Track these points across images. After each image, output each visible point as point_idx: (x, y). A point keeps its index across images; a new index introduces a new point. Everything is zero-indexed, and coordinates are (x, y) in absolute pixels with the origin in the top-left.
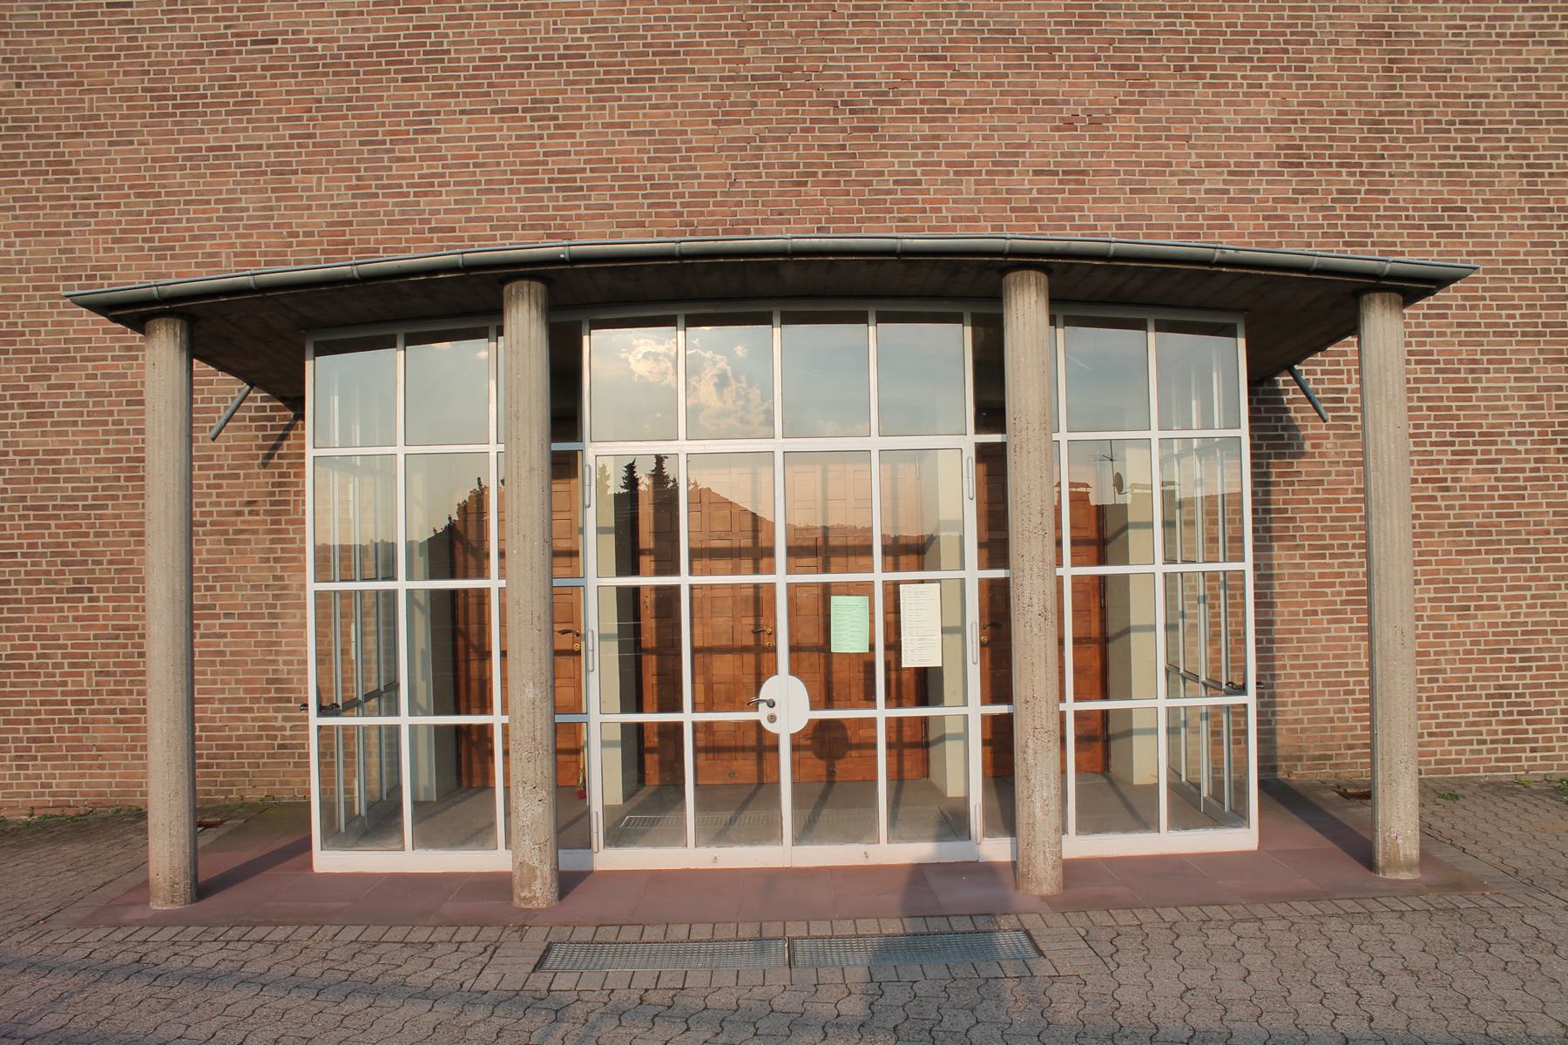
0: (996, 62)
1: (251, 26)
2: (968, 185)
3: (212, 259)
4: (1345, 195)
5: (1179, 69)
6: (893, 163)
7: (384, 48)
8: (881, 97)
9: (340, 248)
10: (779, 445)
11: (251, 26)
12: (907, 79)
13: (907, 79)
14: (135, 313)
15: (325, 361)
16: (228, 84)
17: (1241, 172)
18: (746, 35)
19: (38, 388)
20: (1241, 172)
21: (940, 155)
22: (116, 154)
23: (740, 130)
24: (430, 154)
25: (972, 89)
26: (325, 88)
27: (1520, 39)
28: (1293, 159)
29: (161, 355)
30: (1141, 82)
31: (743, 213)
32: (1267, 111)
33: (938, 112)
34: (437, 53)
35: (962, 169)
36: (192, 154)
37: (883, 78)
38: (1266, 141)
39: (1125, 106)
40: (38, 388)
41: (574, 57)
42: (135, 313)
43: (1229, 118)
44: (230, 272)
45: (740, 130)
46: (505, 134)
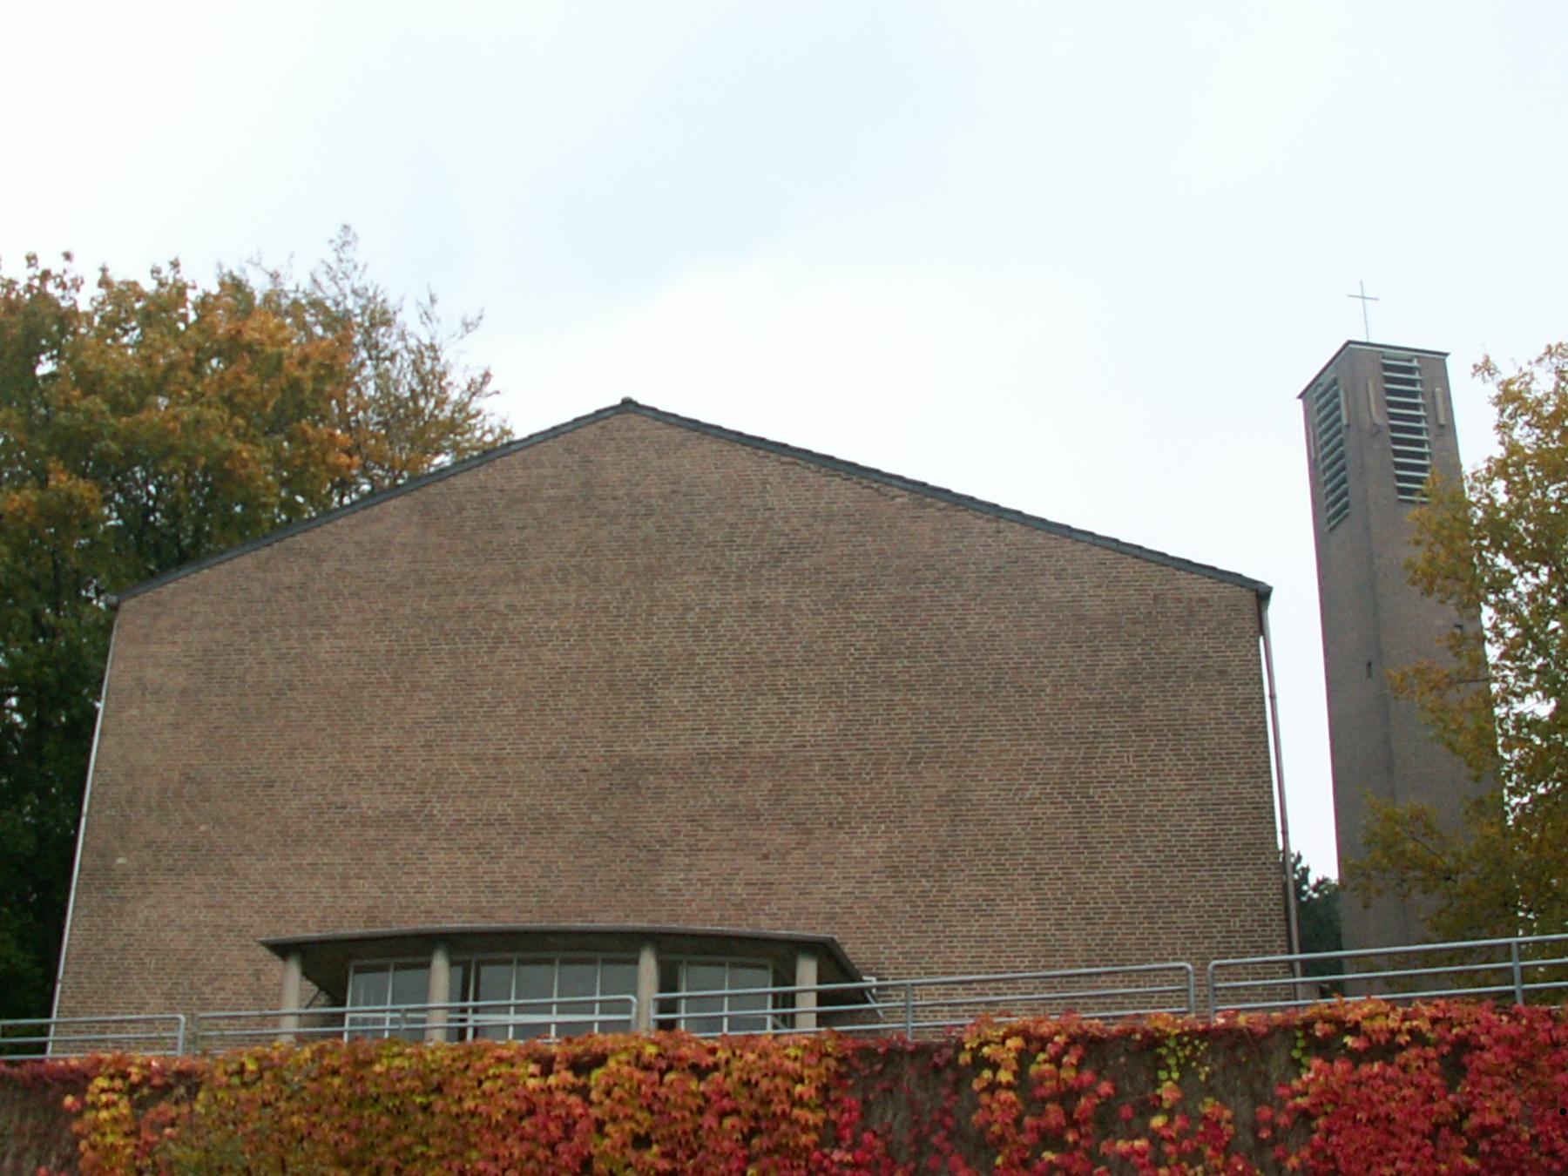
0: (728, 823)
1: (335, 799)
2: (708, 891)
3: (304, 925)
4: (924, 894)
5: (831, 824)
6: (666, 879)
7: (403, 814)
8: (663, 842)
9: (372, 920)
10: (597, 1017)
11: (335, 799)
12: (678, 832)
13: (678, 832)
14: (282, 949)
15: (363, 978)
16: (320, 829)
17: (863, 881)
18: (594, 809)
19: (207, 990)
20: (863, 881)
21: (693, 875)
22: (260, 866)
23: (587, 861)
24: (424, 873)
25: (713, 838)
26: (371, 834)
27: (1033, 802)
28: (894, 872)
29: (292, 972)
30: (809, 832)
31: (586, 906)
32: (880, 846)
33: (693, 850)
34: (430, 816)
35: (705, 882)
36: (299, 867)
37: (664, 831)
38: (878, 864)
39: (800, 845)
40: (207, 990)
41: (502, 820)
42: (282, 949)
43: (858, 852)
44: (312, 933)
45: (587, 861)
46: (463, 861)
